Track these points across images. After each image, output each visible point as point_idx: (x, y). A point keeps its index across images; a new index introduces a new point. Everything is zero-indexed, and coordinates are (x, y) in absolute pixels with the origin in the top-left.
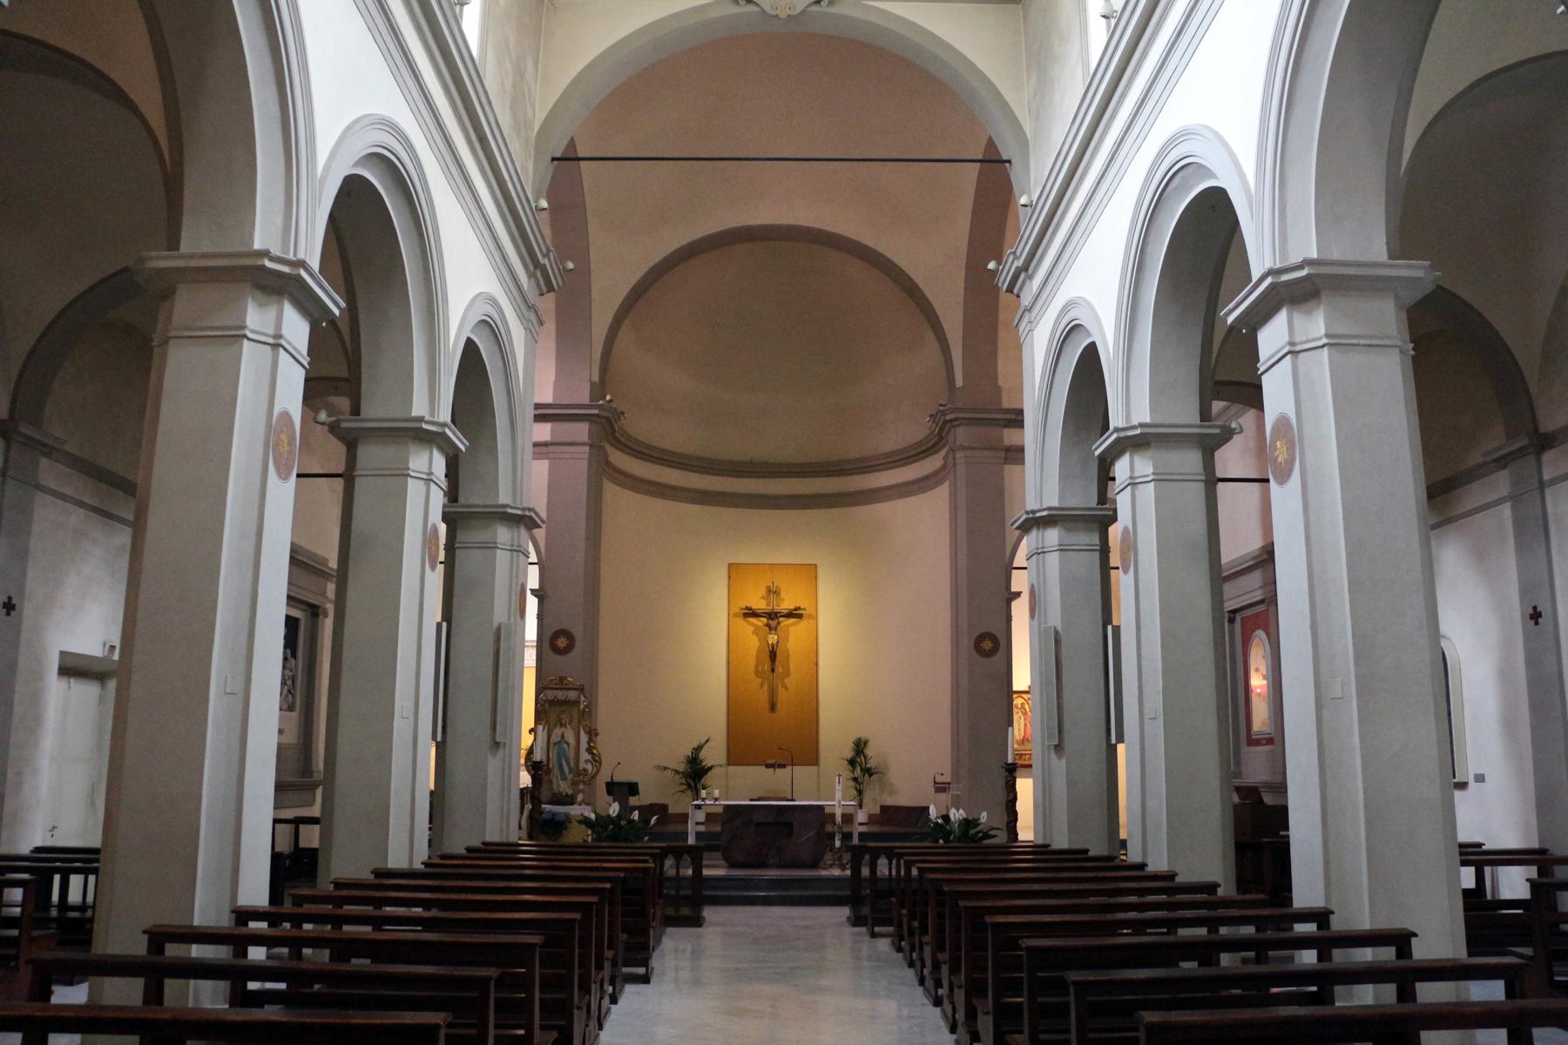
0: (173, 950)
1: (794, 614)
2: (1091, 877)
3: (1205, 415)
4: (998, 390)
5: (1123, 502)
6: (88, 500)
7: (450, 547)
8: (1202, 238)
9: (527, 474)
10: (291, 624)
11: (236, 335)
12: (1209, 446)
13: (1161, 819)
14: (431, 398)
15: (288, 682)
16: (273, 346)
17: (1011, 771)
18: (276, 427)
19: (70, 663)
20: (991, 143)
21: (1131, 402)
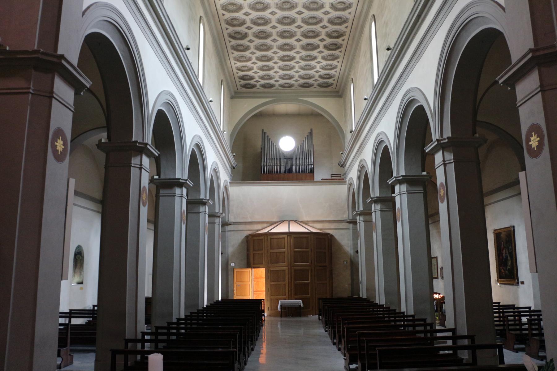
0: (159, 331)
6: (90, 208)
16: (49, 97)
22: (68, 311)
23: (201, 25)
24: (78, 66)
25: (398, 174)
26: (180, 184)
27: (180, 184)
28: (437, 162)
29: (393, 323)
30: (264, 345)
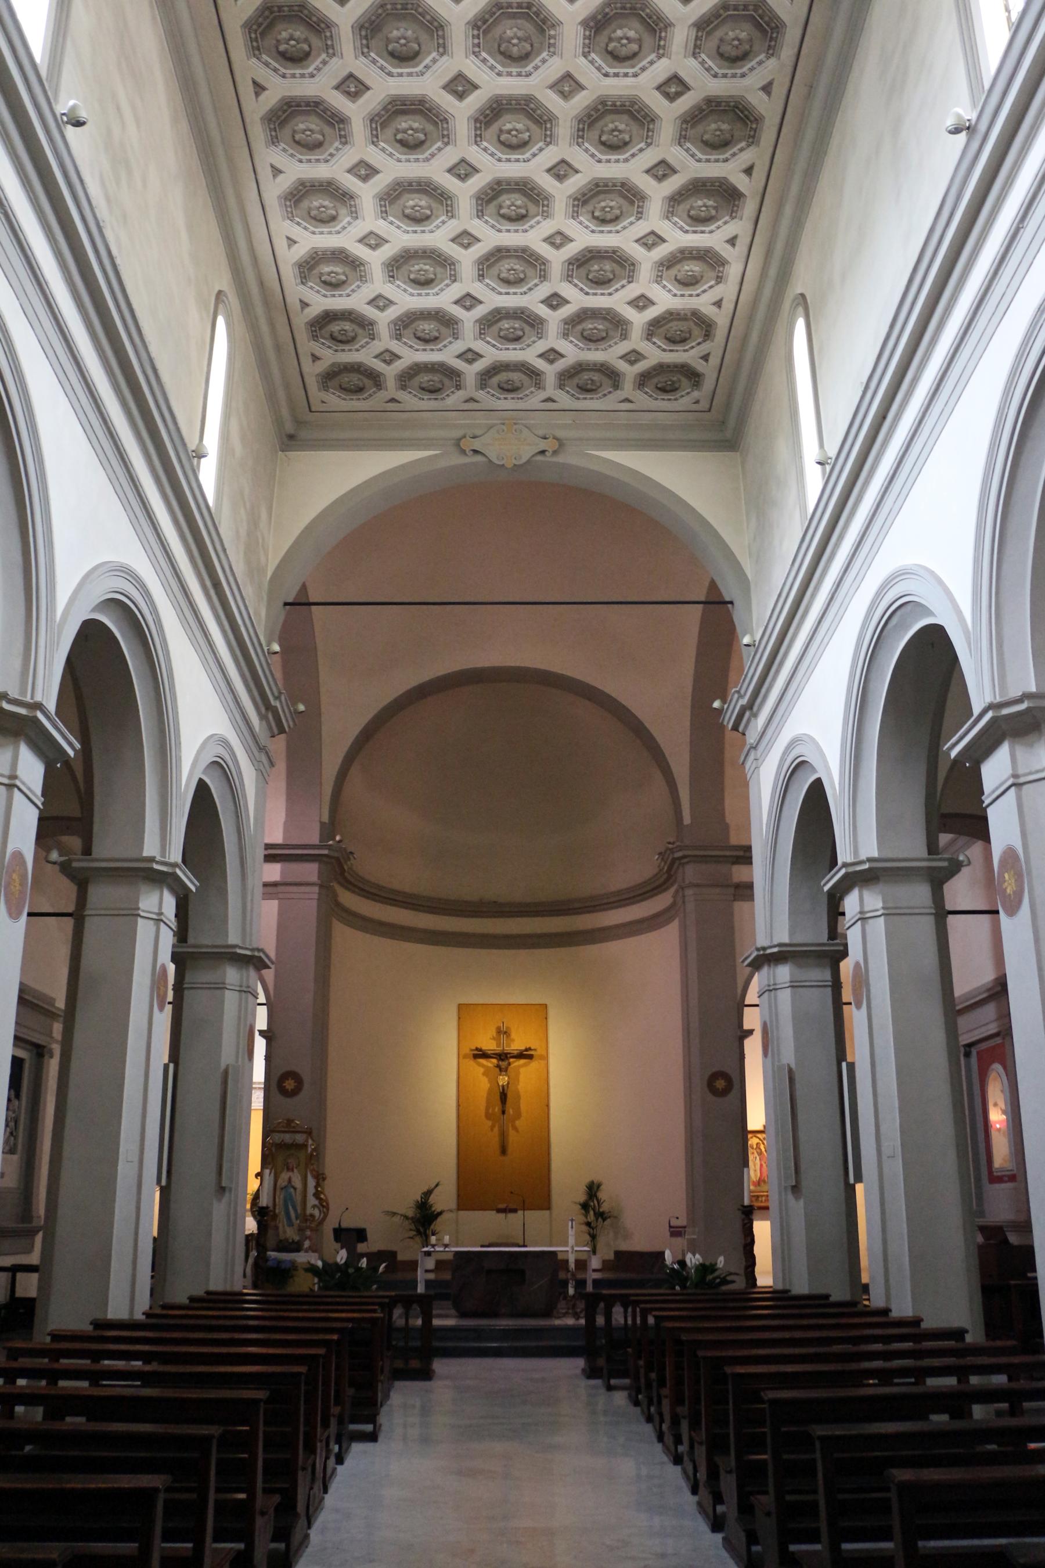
4: (726, 828)
8: (922, 674)
10: (17, 1064)
12: (938, 880)
14: (163, 840)
21: (858, 838)
23: (221, 321)
24: (56, 714)
26: (151, 876)
27: (151, 876)
29: (940, 1419)
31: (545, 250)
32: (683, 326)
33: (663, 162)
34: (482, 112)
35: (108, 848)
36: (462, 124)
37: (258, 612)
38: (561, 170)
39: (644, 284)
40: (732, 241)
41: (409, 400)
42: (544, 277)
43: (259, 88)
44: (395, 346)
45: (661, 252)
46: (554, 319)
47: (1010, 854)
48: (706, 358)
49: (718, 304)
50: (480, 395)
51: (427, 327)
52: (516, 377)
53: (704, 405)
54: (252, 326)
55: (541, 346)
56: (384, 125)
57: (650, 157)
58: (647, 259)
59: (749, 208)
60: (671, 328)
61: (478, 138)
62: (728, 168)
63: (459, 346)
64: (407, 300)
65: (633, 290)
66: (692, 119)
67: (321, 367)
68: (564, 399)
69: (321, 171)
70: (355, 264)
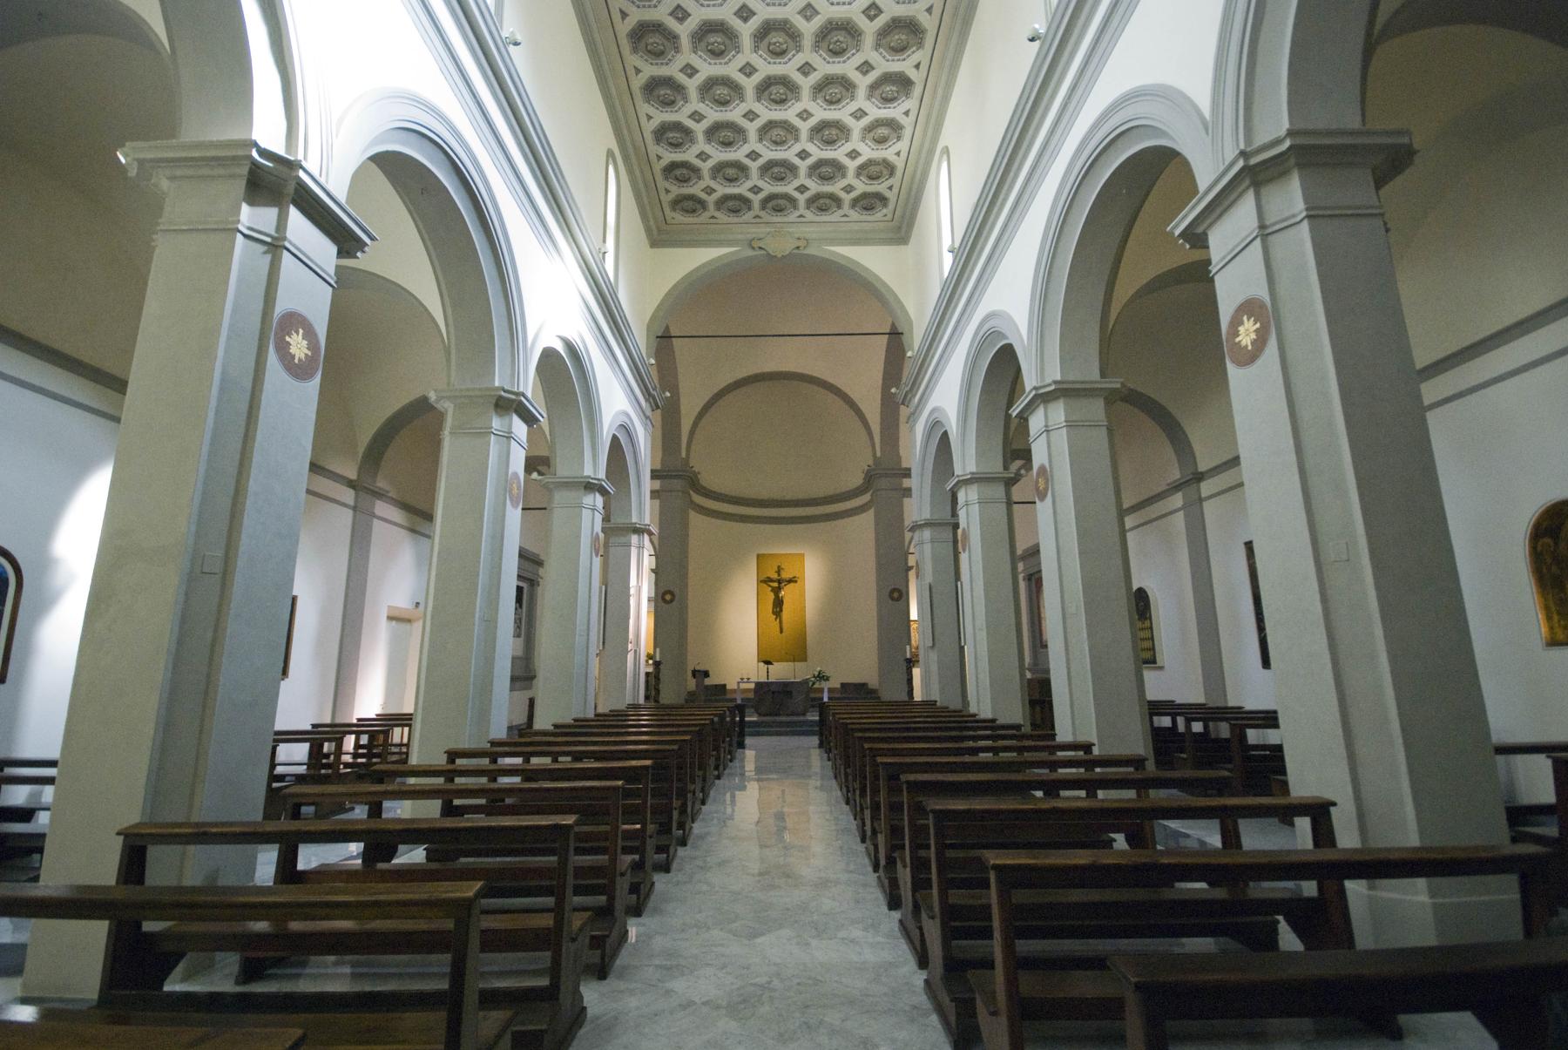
1: (790, 581)
2: (952, 725)
3: (1006, 468)
4: (899, 458)
5: (962, 514)
7: (606, 545)
8: (1002, 366)
9: (644, 509)
10: (519, 590)
11: (487, 432)
12: (1010, 483)
13: (988, 695)
14: (595, 467)
15: (518, 621)
17: (911, 663)
18: (506, 482)
19: (397, 614)
20: (893, 325)
21: (966, 461)
22: (441, 760)
25: (1043, 378)
28: (1032, 432)
30: (947, 242)
31: (797, 122)
32: (877, 168)
33: (866, 62)
34: (758, 30)
35: (563, 469)
36: (752, 135)
37: (640, 338)
38: (806, 69)
39: (855, 142)
40: (907, 113)
41: (722, 217)
42: (797, 139)
43: (638, 71)
44: (713, 184)
45: (865, 121)
46: (803, 166)
47: (1042, 469)
48: (890, 188)
49: (898, 154)
50: (762, 213)
51: (731, 172)
52: (782, 202)
53: (890, 217)
54: (630, 172)
55: (796, 183)
56: (700, 40)
57: (857, 60)
58: (857, 127)
59: (917, 91)
60: (871, 170)
61: (756, 49)
62: (903, 65)
63: (749, 184)
64: (719, 155)
65: (848, 147)
66: (884, 32)
67: (671, 196)
68: (809, 216)
69: (664, 71)
70: (687, 132)
